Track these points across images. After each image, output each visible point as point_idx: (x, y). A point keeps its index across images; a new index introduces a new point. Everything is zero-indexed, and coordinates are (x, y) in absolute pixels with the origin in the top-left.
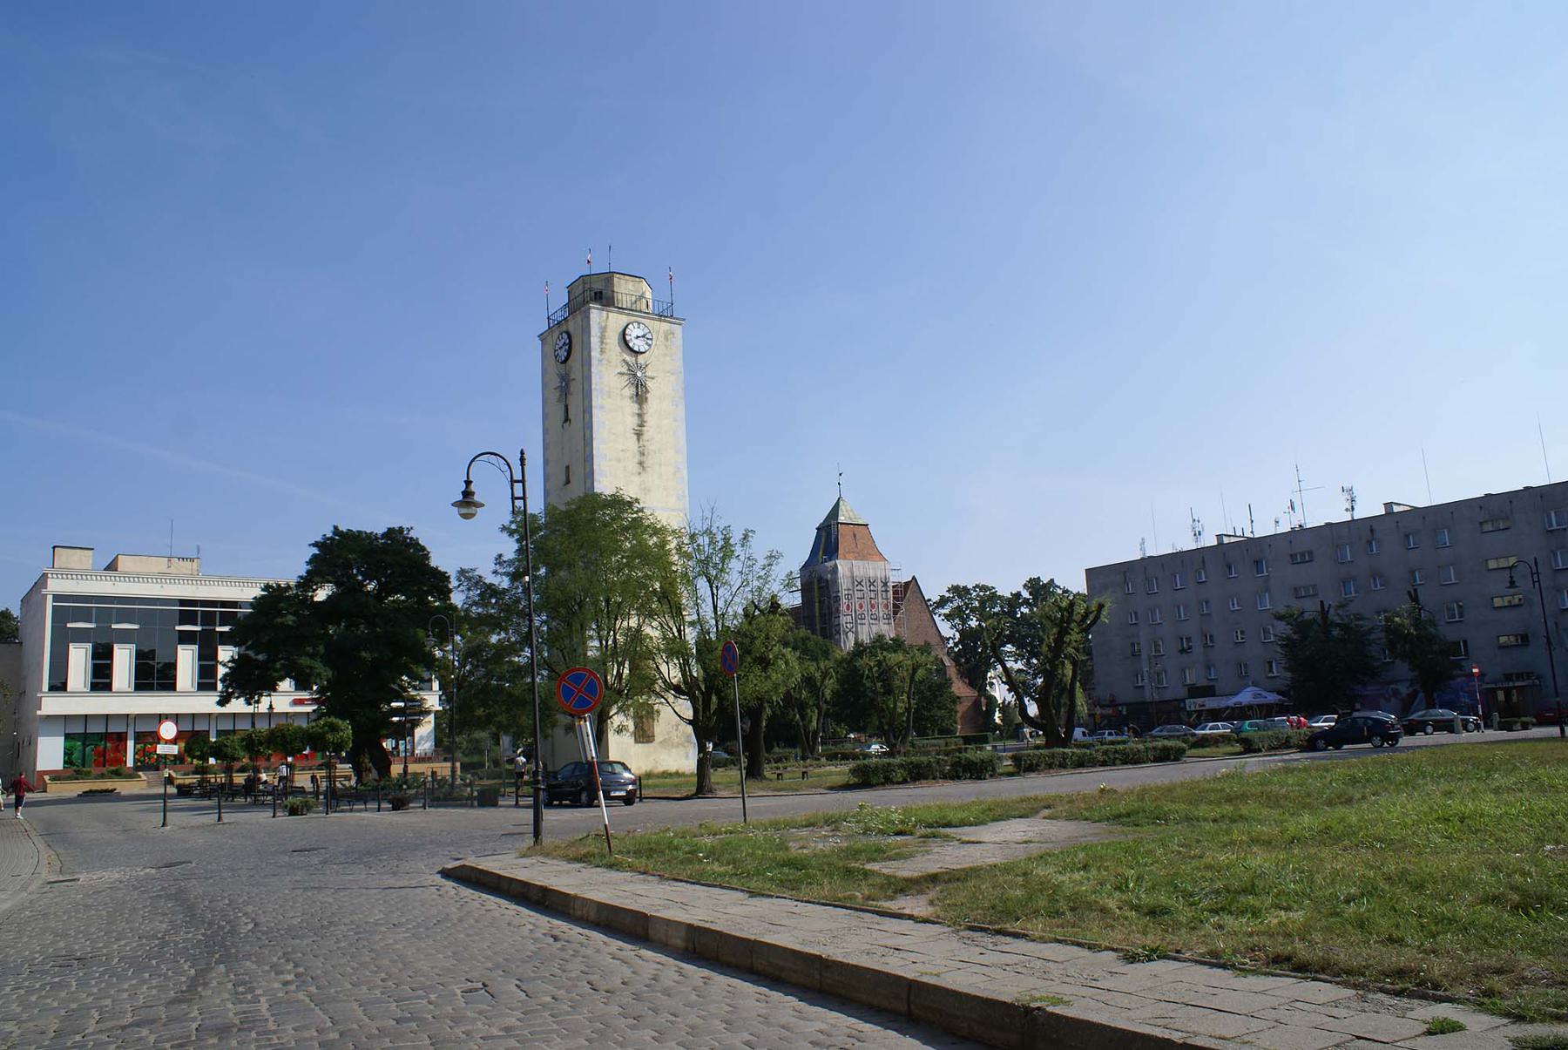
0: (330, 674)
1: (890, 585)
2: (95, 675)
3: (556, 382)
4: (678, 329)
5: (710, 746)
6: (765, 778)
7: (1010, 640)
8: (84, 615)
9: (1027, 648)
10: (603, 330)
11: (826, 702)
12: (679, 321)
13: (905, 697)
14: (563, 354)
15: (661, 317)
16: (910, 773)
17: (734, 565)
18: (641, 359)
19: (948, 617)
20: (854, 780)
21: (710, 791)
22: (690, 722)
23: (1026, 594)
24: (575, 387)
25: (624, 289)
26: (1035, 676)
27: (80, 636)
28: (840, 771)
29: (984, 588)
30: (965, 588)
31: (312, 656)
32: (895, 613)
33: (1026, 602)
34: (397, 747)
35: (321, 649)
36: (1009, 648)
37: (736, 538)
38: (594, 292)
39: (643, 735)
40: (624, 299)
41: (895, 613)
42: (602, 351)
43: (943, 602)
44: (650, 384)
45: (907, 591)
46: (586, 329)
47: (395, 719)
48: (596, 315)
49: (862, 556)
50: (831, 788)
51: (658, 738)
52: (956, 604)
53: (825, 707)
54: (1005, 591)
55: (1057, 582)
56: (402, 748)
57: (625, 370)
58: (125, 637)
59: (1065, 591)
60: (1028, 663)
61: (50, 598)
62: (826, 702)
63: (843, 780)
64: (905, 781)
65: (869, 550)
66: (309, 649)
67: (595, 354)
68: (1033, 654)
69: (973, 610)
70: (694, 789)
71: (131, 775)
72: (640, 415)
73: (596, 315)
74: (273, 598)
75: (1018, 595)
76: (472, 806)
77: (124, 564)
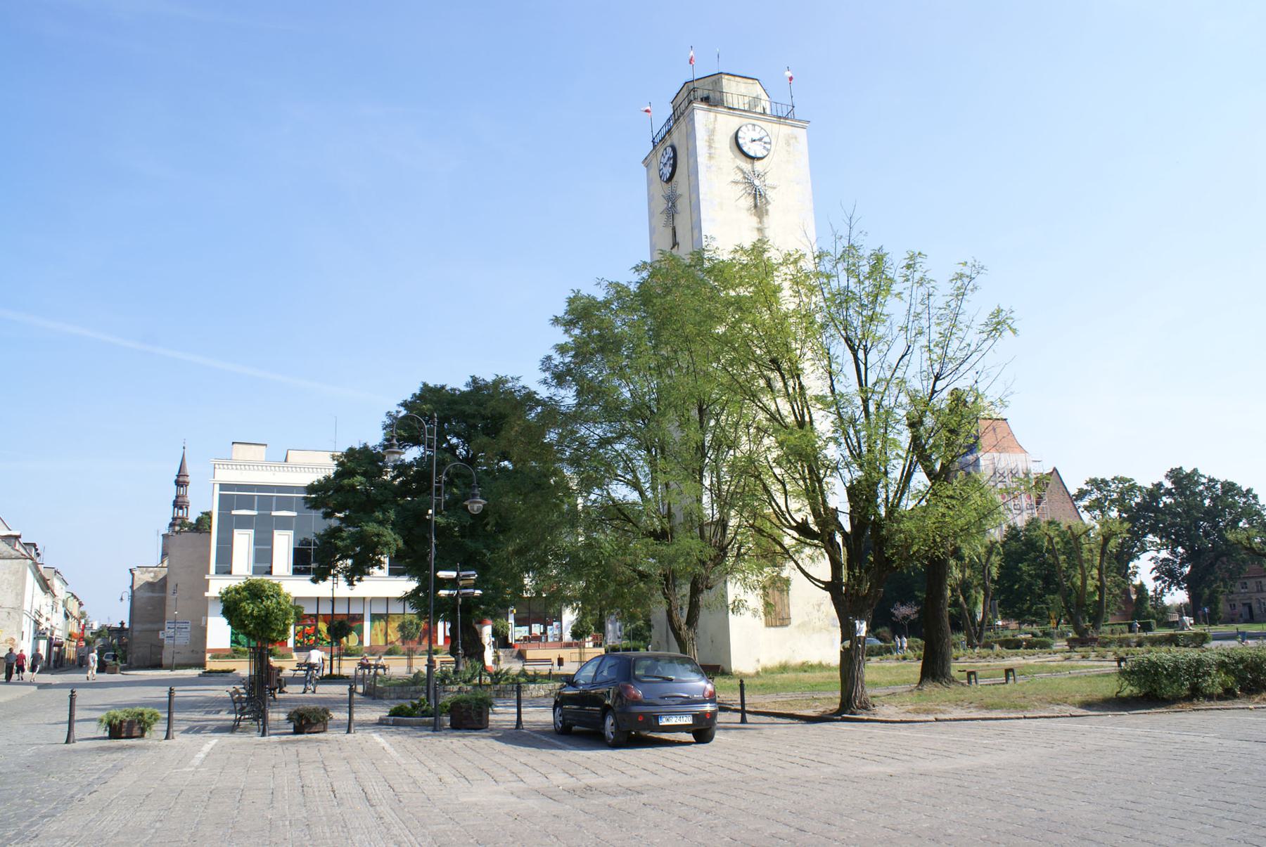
0: (401, 543)
1: (1032, 476)
2: (295, 562)
3: (662, 205)
4: (802, 134)
5: (862, 628)
6: (953, 680)
7: (1154, 530)
8: (247, 503)
9: (1171, 537)
10: (712, 133)
11: (993, 581)
12: (804, 123)
13: (1095, 572)
14: (667, 170)
15: (780, 119)
16: (1241, 679)
17: (894, 308)
18: (758, 165)
19: (1087, 508)
20: (1129, 690)
21: (865, 707)
22: (828, 586)
23: (1168, 484)
24: (682, 205)
25: (734, 90)
26: (1182, 565)
27: (244, 523)
28: (1098, 669)
29: (1122, 480)
30: (1103, 481)
31: (381, 523)
32: (1038, 503)
33: (1169, 493)
34: (545, 632)
35: (392, 515)
36: (1150, 537)
37: (895, 268)
38: (703, 93)
39: (776, 615)
40: (731, 100)
41: (1038, 503)
42: (711, 157)
43: (1082, 494)
44: (770, 194)
45: (1047, 484)
46: (691, 135)
47: (443, 593)
48: (702, 116)
49: (998, 447)
50: (1088, 705)
51: (795, 620)
52: (1094, 497)
53: (992, 586)
54: (1146, 482)
55: (1201, 472)
56: (549, 633)
57: (739, 177)
58: (284, 524)
59: (1211, 480)
60: (1173, 552)
61: (217, 487)
62: (993, 581)
63: (1109, 688)
64: (1228, 694)
65: (1007, 443)
66: (379, 515)
67: (702, 159)
68: (1176, 543)
69: (1112, 501)
70: (832, 700)
71: (1025, 640)
72: (760, 230)
73: (702, 116)
74: (357, 462)
75: (1160, 485)
76: (436, 728)
77: (294, 457)
